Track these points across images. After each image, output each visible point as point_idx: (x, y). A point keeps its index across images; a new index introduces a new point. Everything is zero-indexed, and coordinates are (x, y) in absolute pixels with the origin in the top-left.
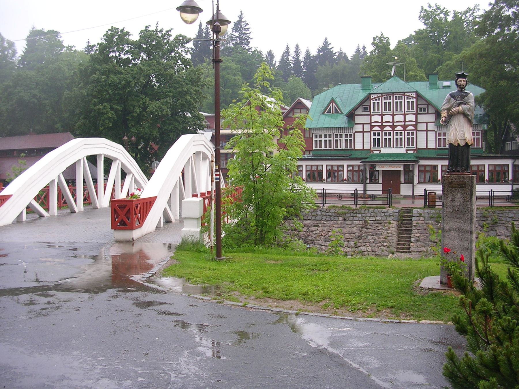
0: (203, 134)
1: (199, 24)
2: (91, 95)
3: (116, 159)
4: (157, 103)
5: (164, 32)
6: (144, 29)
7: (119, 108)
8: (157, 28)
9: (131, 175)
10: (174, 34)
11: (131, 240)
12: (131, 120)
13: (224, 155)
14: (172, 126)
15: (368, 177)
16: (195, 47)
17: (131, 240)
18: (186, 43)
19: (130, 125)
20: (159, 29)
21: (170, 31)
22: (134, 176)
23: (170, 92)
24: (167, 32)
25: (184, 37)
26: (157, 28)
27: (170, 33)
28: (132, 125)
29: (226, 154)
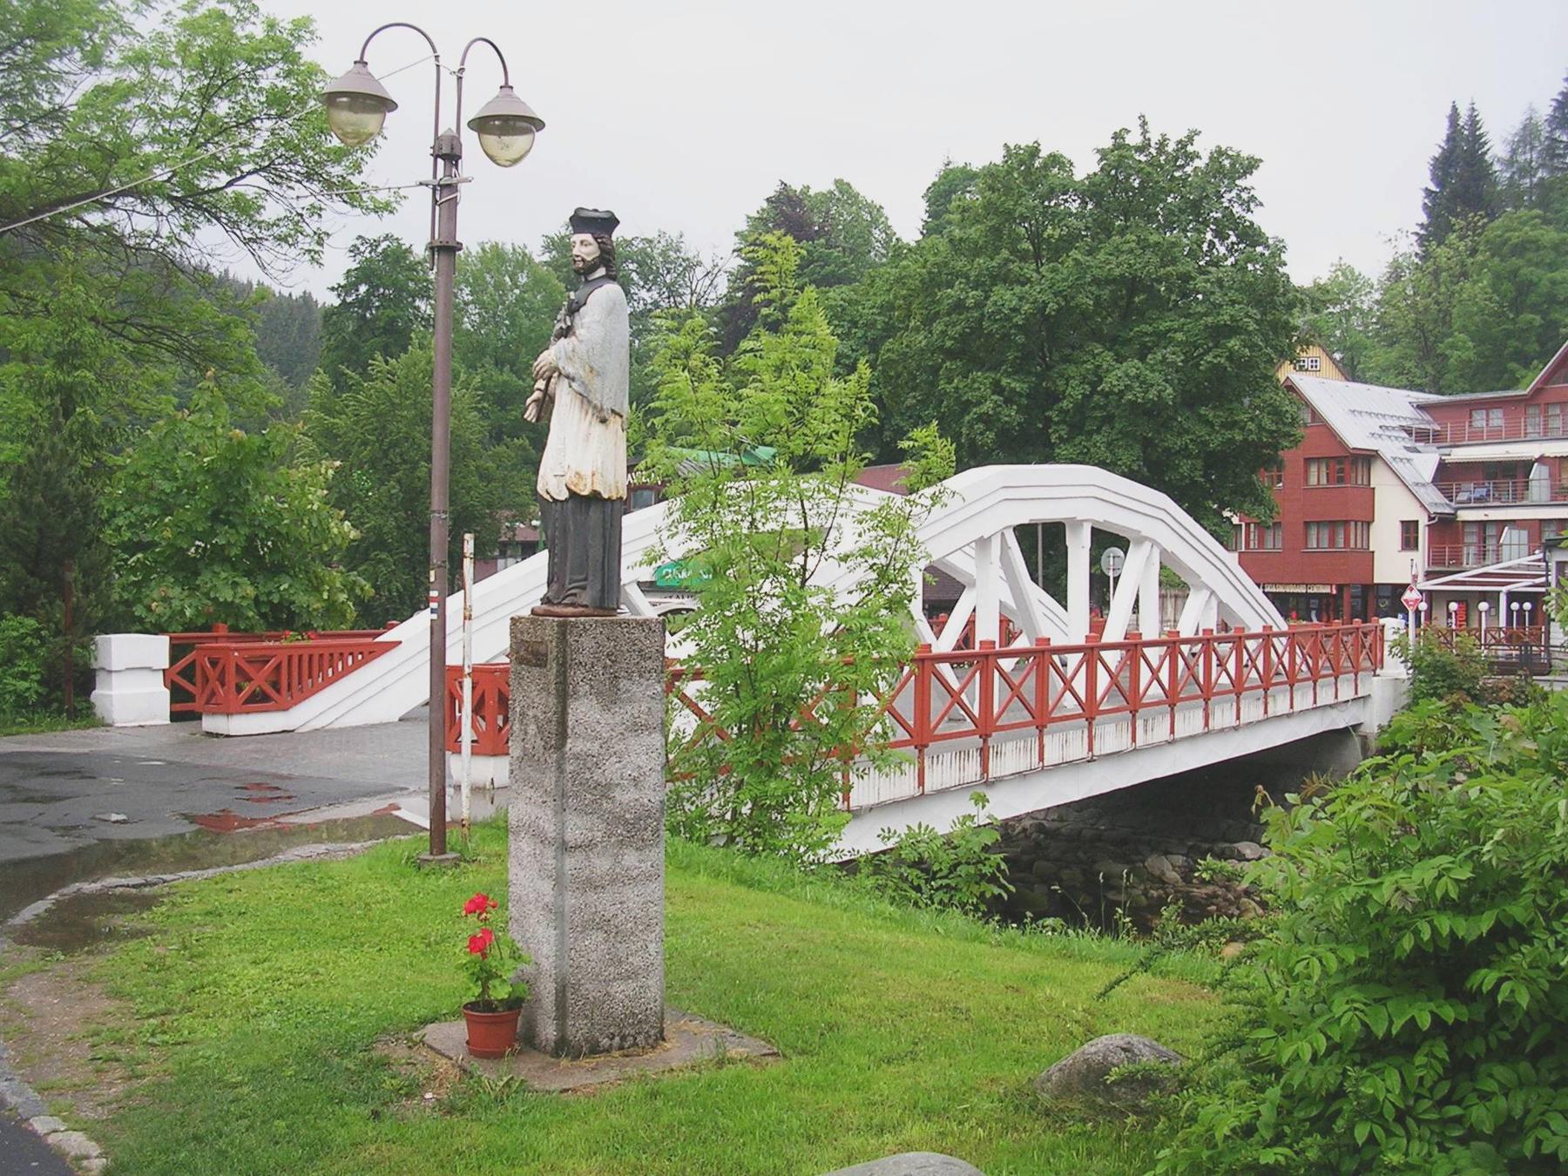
0: (1408, 460)
1: (1448, 111)
2: (941, 348)
3: (1142, 540)
4: (1132, 366)
5: (1171, 147)
6: (1108, 143)
7: (1017, 386)
8: (1148, 136)
9: (1206, 593)
10: (1203, 147)
11: (488, 786)
12: (1057, 423)
13: (1475, 529)
14: (1187, 438)
15: (1315, 590)
16: (1438, 185)
17: (488, 786)
18: (1245, 174)
19: (1053, 438)
20: (1155, 138)
21: (1190, 139)
22: (1217, 596)
23: (1180, 330)
24: (1182, 145)
25: (1235, 159)
26: (1148, 136)
27: (1190, 149)
28: (1060, 438)
29: (1483, 525)
